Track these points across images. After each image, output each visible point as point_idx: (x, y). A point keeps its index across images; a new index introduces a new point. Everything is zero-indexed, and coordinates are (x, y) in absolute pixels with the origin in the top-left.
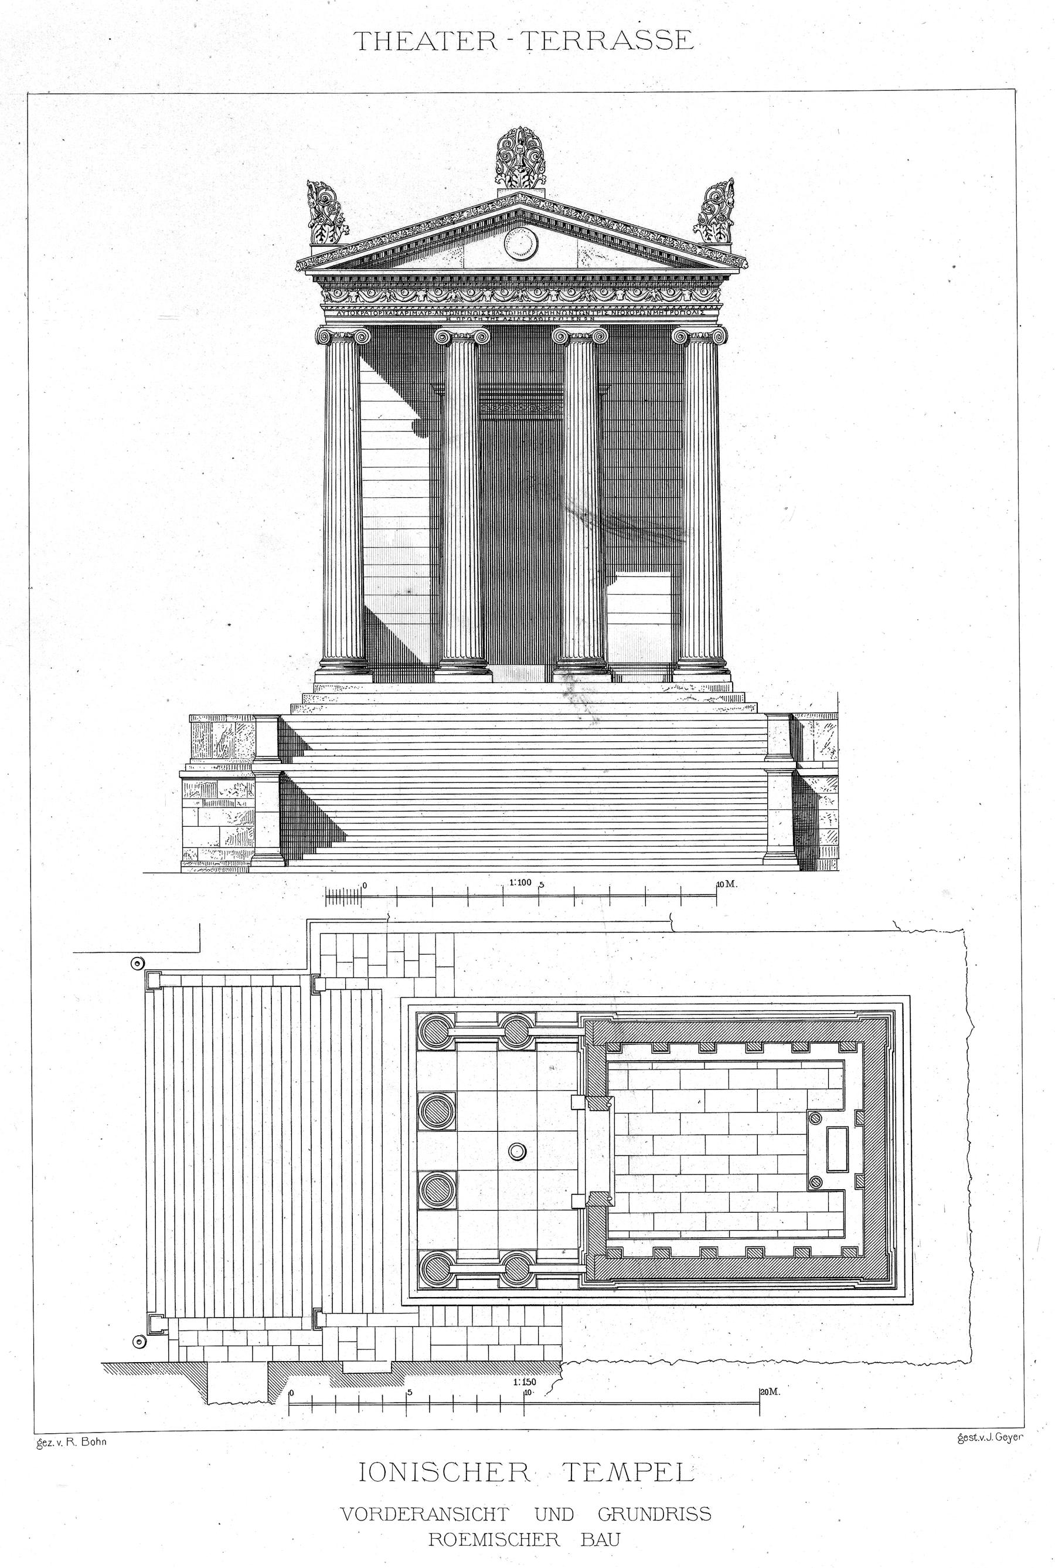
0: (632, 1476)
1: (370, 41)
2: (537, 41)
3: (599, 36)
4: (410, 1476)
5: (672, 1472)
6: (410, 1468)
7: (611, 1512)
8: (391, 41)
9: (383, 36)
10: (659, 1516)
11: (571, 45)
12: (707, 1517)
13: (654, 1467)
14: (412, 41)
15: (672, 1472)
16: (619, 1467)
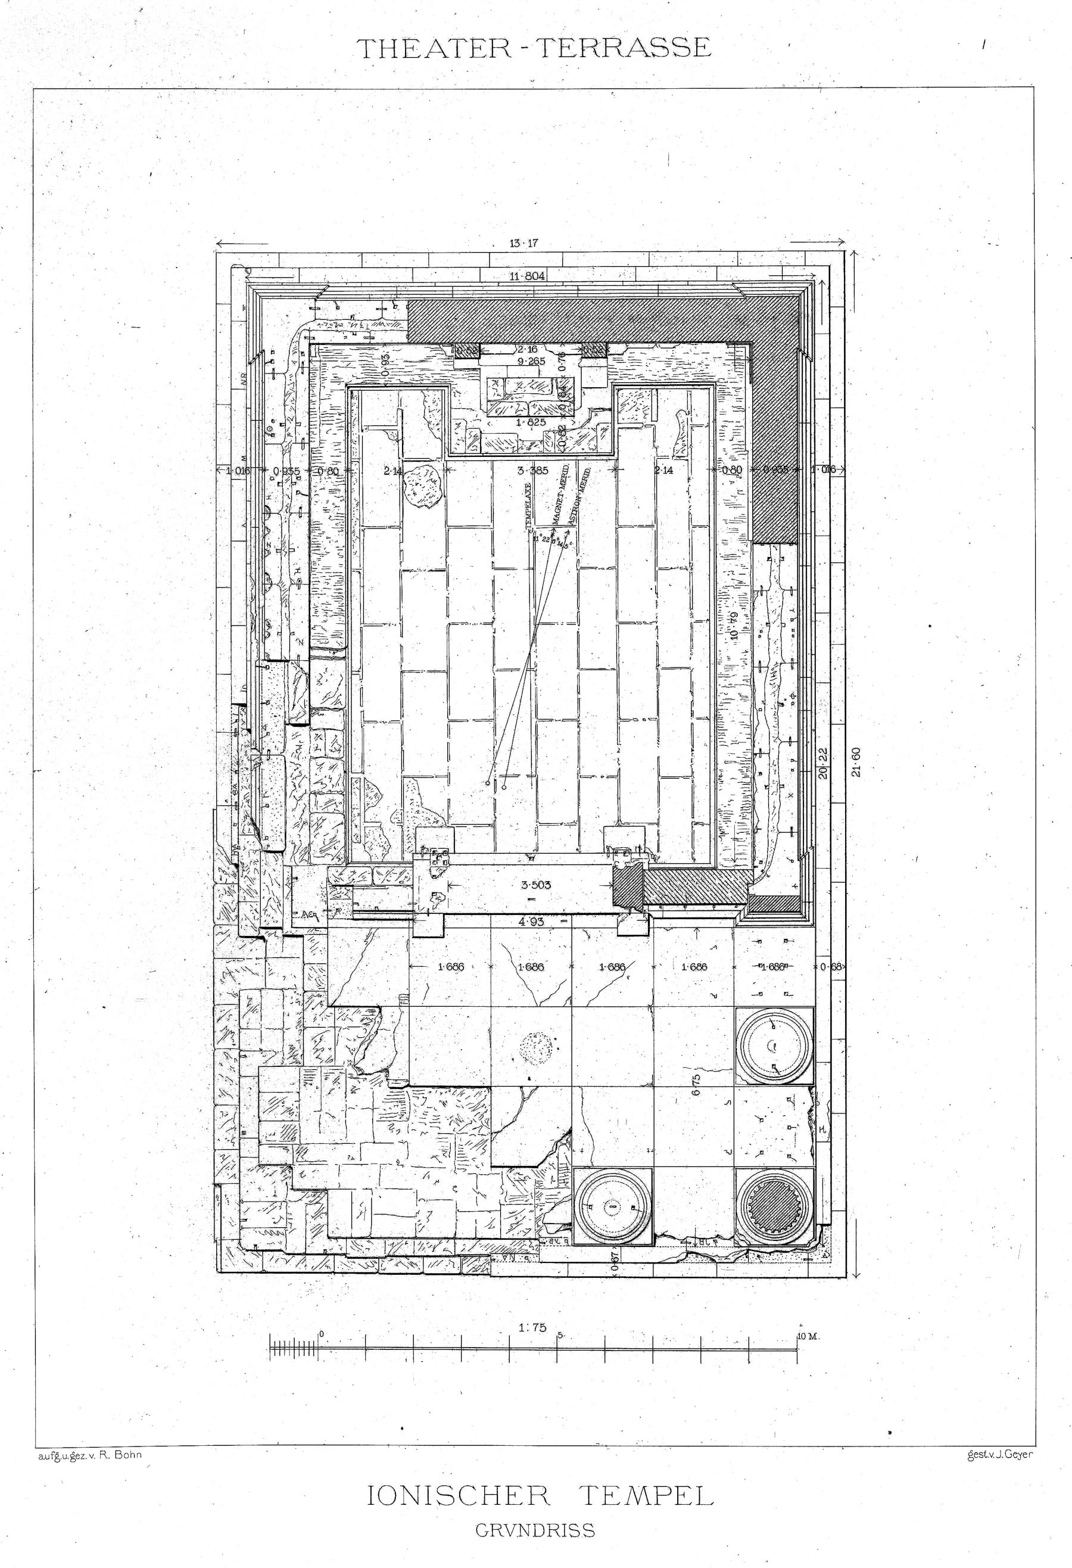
0: (653, 1500)
1: (374, 49)
2: (553, 48)
3: (616, 43)
4: (423, 1499)
5: (692, 1496)
6: (423, 1491)
7: (489, 1528)
8: (403, 48)
9: (388, 44)
10: (539, 1532)
11: (589, 52)
12: (590, 1534)
13: (674, 1490)
14: (422, 48)
15: (692, 1496)
16: (638, 1491)
